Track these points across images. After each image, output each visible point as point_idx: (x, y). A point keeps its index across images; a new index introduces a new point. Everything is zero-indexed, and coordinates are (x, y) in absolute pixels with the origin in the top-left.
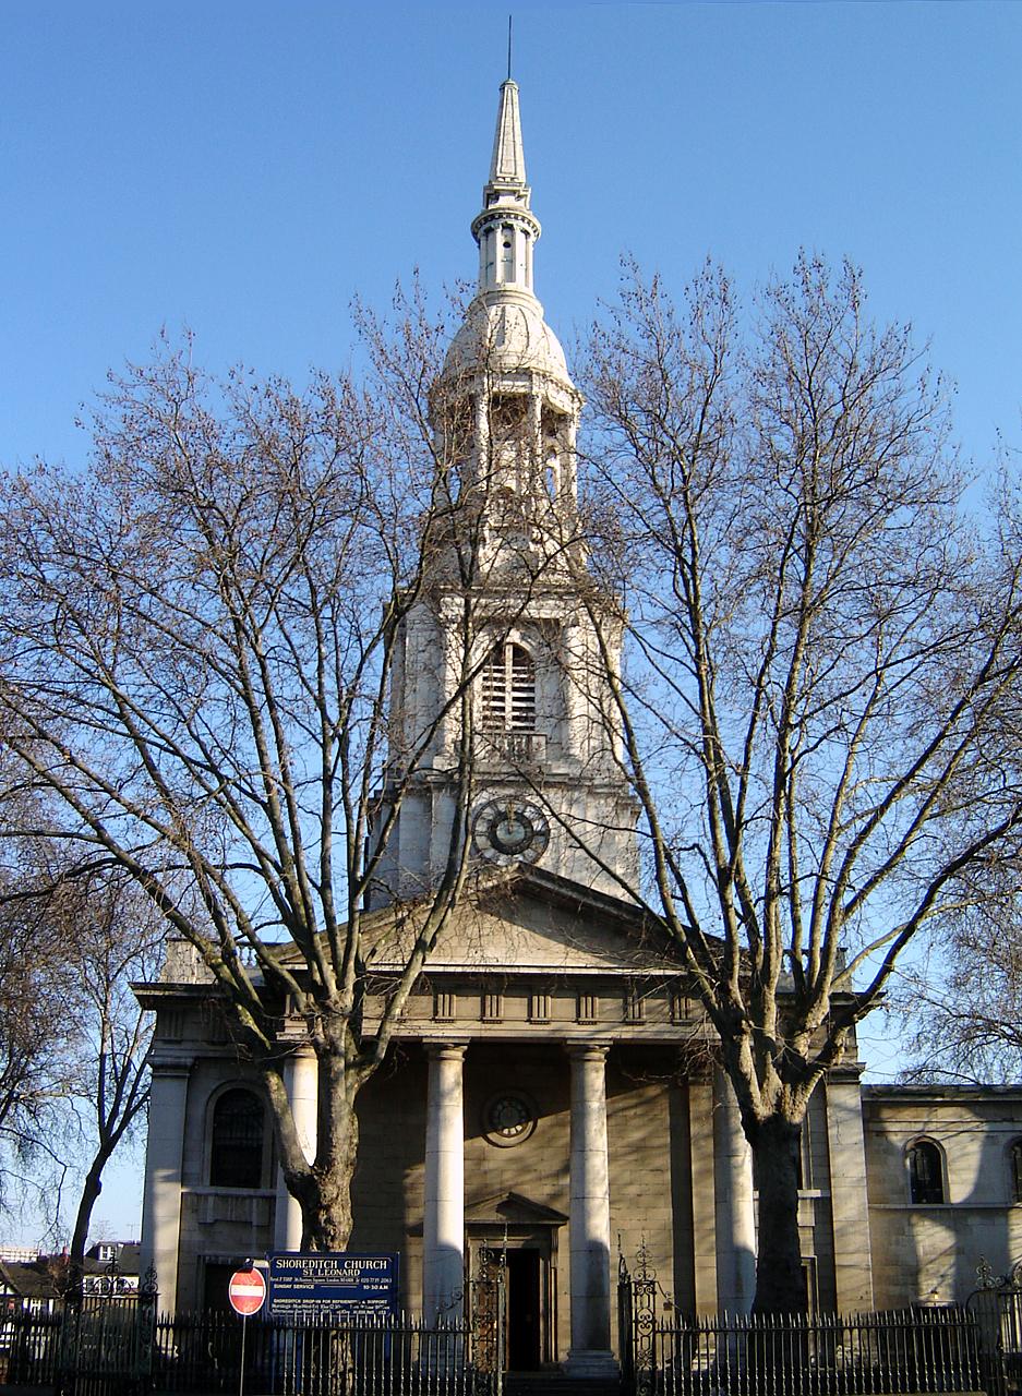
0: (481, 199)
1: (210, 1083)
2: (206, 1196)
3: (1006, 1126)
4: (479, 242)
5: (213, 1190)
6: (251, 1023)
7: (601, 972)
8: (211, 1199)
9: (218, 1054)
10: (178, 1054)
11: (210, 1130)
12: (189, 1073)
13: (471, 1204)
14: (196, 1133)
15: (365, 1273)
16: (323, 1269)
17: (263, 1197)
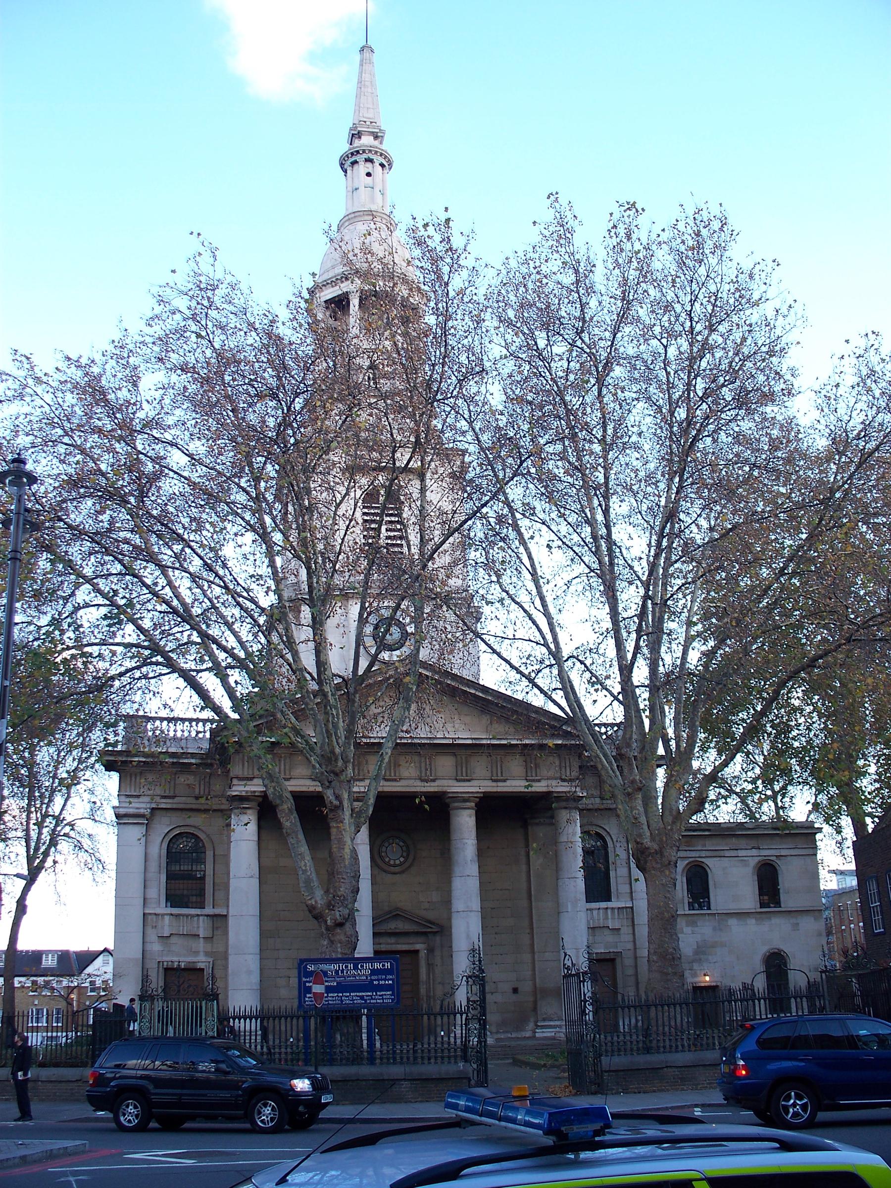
0: (345, 136)
1: (163, 828)
2: (163, 915)
3: (754, 852)
4: (346, 171)
5: (170, 910)
6: (660, 784)
7: (474, 742)
8: (167, 918)
9: (169, 806)
10: (137, 805)
11: (164, 865)
12: (147, 820)
13: (377, 921)
14: (153, 866)
15: (374, 972)
16: (342, 971)
17: (207, 916)
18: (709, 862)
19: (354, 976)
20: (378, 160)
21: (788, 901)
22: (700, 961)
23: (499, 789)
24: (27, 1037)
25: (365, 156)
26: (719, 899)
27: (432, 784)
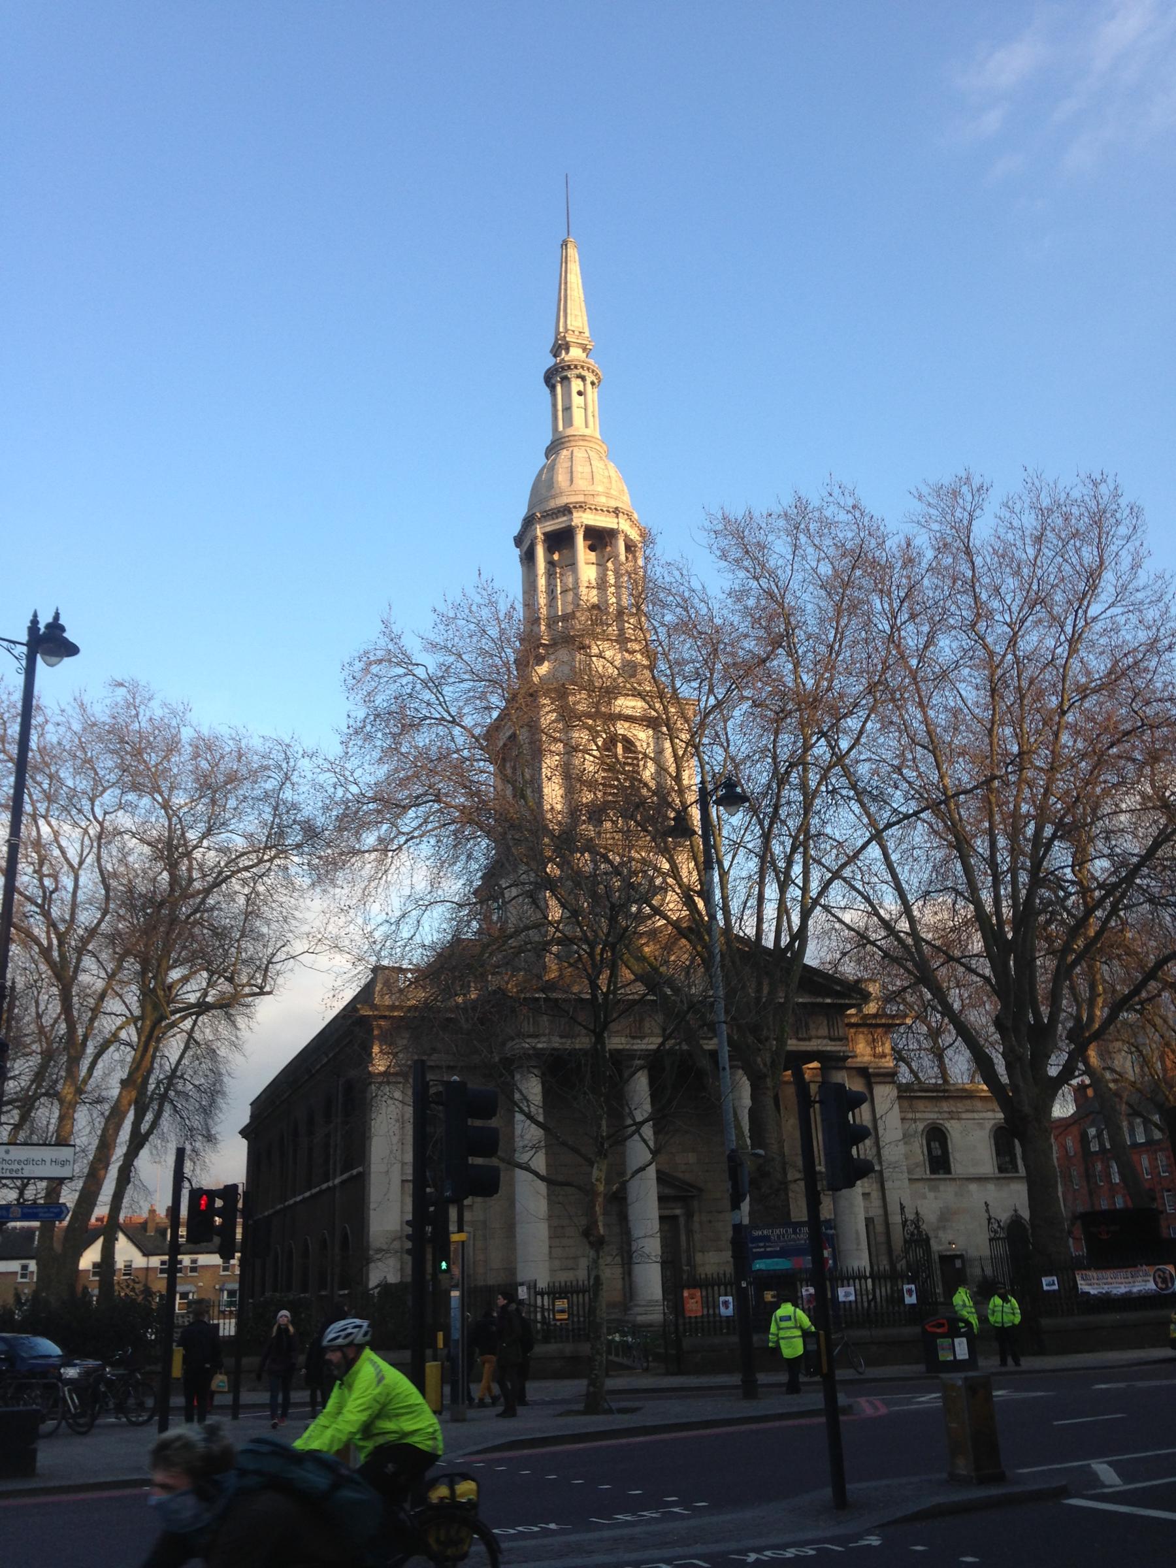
18: (948, 1125)
19: (794, 1240)
20: (590, 377)
21: (957, 1168)
22: (944, 1228)
23: (803, 1048)
24: (218, 1325)
25: (577, 372)
26: (960, 1163)
27: (807, 1043)
